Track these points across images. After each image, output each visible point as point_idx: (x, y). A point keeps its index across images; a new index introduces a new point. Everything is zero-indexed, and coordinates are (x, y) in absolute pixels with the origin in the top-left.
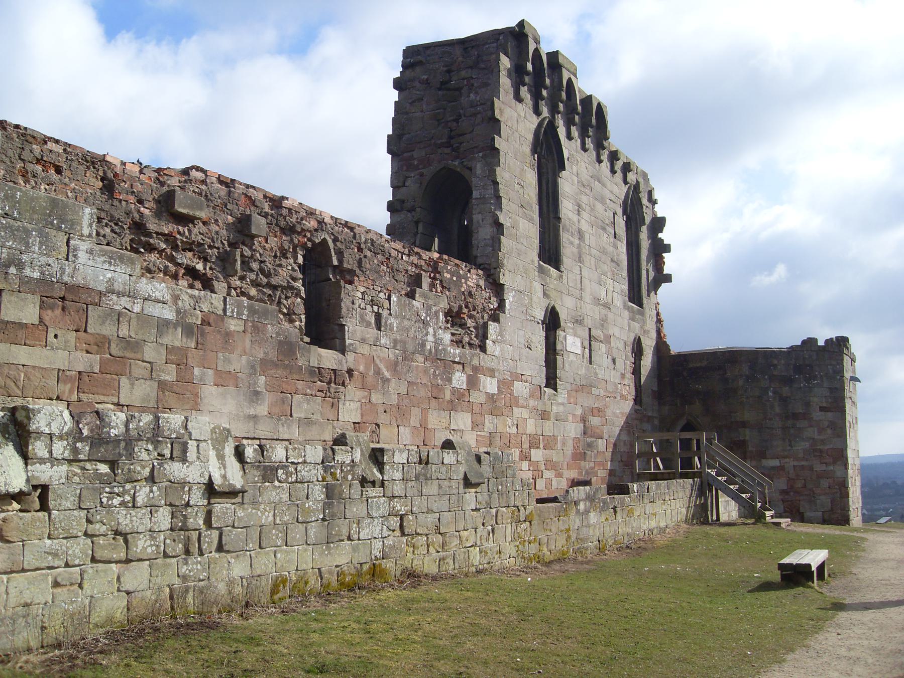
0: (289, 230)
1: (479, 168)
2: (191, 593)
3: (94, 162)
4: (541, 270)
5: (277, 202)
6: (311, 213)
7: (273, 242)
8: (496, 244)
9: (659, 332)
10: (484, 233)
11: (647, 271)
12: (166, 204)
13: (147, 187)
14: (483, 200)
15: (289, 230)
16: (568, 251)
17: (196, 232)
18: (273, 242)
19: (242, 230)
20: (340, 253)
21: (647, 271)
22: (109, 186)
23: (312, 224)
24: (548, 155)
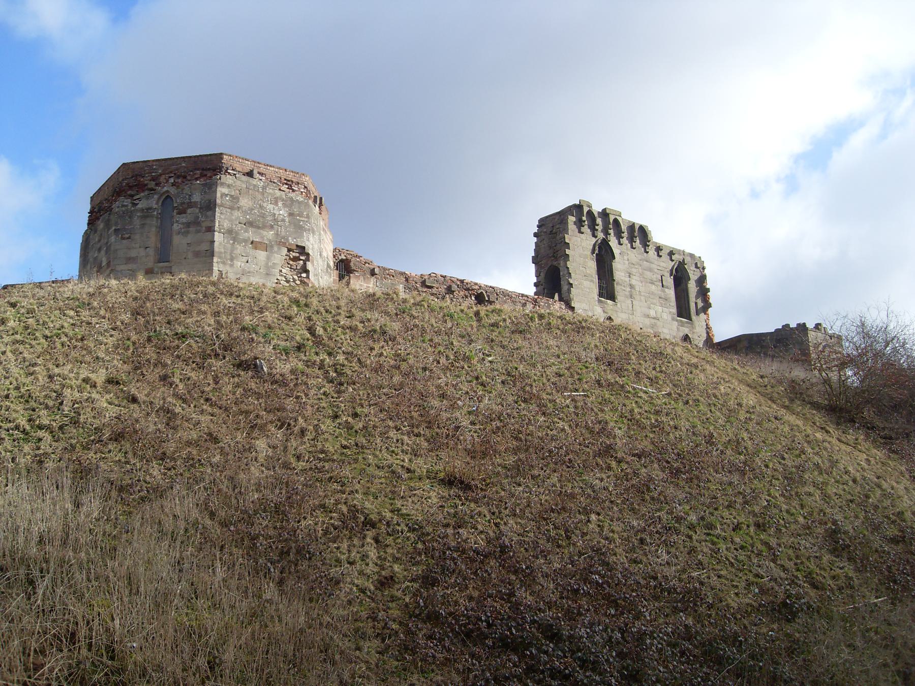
0: (468, 289)
1: (562, 263)
2: (104, 264)
3: (402, 274)
4: (600, 301)
5: (462, 281)
6: (476, 284)
7: (462, 293)
8: (569, 291)
9: (708, 333)
10: (565, 287)
11: (696, 303)
12: (424, 284)
13: (420, 281)
14: (564, 275)
15: (468, 289)
16: (669, 281)
17: (434, 291)
18: (462, 293)
19: (449, 290)
20: (488, 296)
21: (696, 303)
22: (407, 280)
23: (477, 287)
24: (604, 257)
